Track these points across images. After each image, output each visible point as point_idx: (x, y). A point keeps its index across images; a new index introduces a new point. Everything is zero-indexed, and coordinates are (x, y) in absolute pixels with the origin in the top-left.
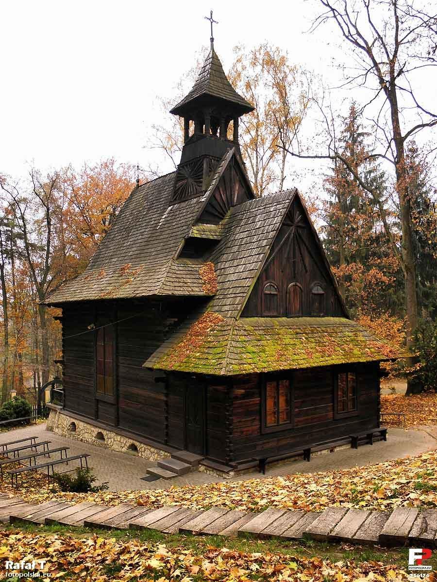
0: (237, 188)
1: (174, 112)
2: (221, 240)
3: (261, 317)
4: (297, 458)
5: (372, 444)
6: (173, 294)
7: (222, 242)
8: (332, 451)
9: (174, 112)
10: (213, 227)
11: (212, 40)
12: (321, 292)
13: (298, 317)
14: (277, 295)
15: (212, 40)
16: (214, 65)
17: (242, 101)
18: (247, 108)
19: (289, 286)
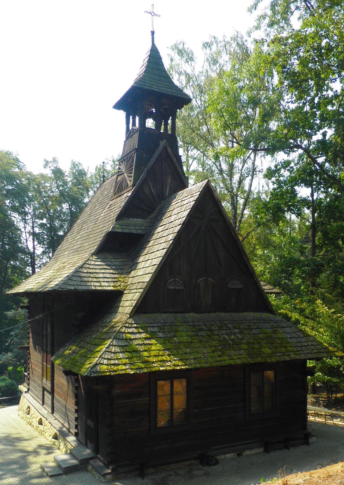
0: (169, 181)
1: (119, 106)
2: (145, 234)
3: (163, 313)
4: (193, 462)
5: (288, 449)
6: (75, 289)
7: (146, 236)
8: (239, 455)
9: (119, 106)
10: (140, 221)
11: (153, 33)
12: (240, 286)
13: (209, 312)
14: (183, 290)
15: (153, 33)
16: (154, 57)
17: (178, 92)
18: (187, 100)
19: (198, 281)
